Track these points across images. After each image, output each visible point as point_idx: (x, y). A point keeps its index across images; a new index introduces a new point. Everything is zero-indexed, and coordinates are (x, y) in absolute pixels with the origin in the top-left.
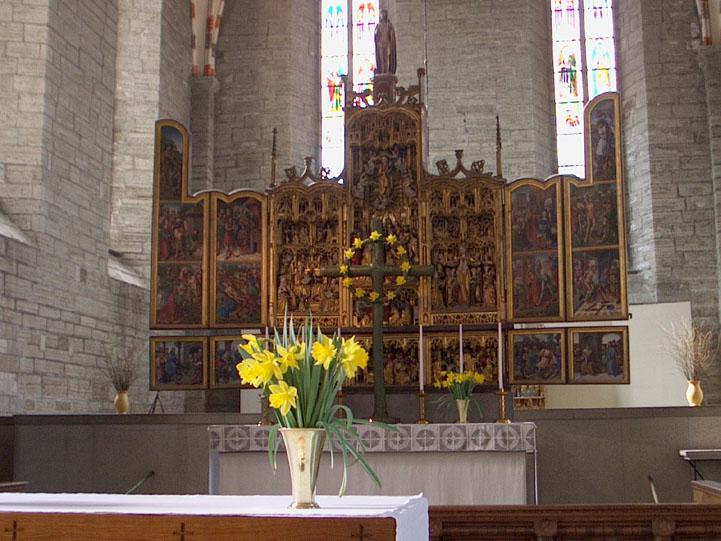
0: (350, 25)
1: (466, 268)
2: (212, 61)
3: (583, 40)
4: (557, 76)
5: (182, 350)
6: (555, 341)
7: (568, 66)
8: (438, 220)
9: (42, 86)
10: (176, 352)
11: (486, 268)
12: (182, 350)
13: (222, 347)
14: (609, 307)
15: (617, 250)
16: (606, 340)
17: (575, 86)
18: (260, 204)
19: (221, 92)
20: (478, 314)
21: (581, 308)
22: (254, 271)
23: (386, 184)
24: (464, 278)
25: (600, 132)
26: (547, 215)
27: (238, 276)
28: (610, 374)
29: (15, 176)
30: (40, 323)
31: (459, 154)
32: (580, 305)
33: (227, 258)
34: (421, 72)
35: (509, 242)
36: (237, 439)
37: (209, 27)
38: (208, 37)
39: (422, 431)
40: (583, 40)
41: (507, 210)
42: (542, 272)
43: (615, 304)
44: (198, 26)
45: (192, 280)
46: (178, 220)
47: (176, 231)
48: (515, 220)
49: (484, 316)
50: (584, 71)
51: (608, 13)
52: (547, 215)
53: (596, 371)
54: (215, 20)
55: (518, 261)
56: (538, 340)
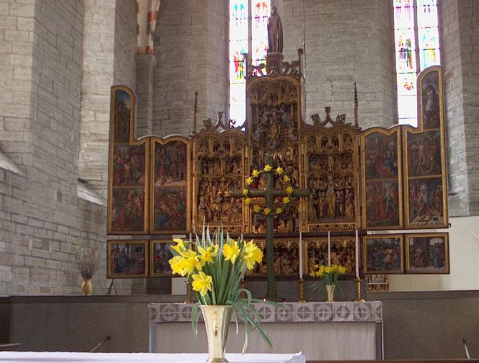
0: (250, 18)
1: (333, 191)
2: (151, 44)
3: (416, 29)
4: (398, 54)
5: (130, 249)
6: (396, 243)
7: (405, 47)
8: (313, 157)
9: (30, 61)
10: (126, 251)
11: (347, 191)
12: (130, 249)
13: (159, 247)
14: (434, 219)
15: (441, 178)
16: (432, 242)
17: (410, 61)
18: (186, 145)
19: (158, 66)
20: (341, 224)
21: (415, 220)
22: (182, 193)
23: (276, 131)
24: (331, 198)
25: (428, 94)
26: (391, 153)
27: (170, 197)
28: (435, 267)
29: (11, 126)
30: (29, 230)
31: (328, 110)
32: (414, 218)
33: (162, 184)
34: (301, 51)
35: (363, 173)
36: (169, 313)
37: (149, 19)
38: (149, 27)
39: (302, 308)
40: (416, 29)
41: (362, 150)
42: (387, 194)
43: (439, 217)
44: (141, 19)
45: (137, 200)
46: (127, 157)
47: (126, 165)
48: (367, 157)
49: (345, 226)
50: (417, 51)
51: (434, 9)
52: (391, 153)
53: (426, 264)
54: (153, 14)
55: (370, 186)
56: (384, 242)
